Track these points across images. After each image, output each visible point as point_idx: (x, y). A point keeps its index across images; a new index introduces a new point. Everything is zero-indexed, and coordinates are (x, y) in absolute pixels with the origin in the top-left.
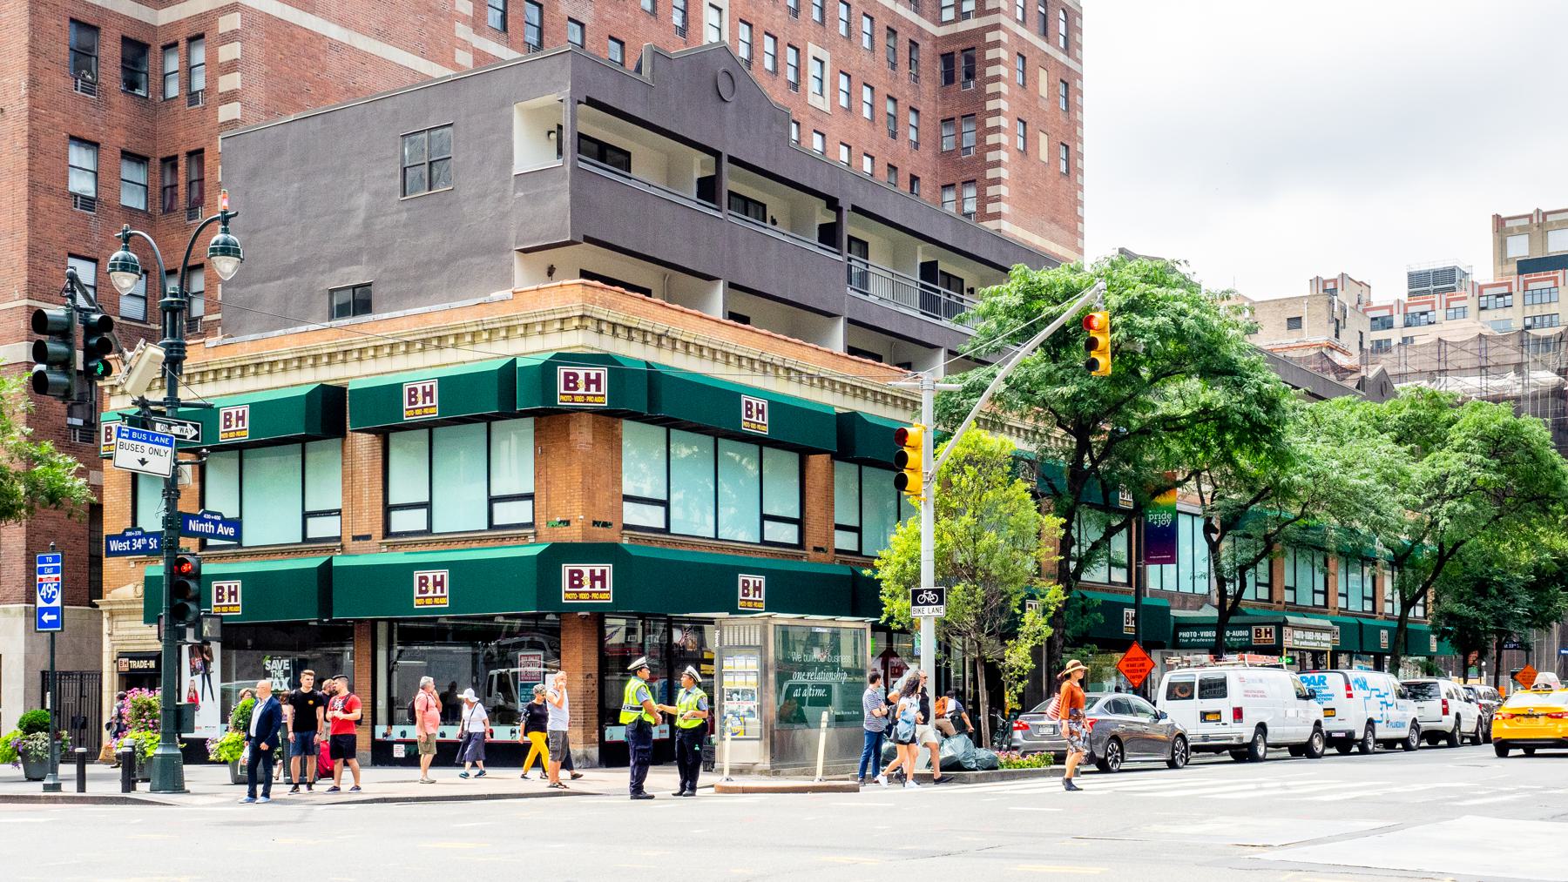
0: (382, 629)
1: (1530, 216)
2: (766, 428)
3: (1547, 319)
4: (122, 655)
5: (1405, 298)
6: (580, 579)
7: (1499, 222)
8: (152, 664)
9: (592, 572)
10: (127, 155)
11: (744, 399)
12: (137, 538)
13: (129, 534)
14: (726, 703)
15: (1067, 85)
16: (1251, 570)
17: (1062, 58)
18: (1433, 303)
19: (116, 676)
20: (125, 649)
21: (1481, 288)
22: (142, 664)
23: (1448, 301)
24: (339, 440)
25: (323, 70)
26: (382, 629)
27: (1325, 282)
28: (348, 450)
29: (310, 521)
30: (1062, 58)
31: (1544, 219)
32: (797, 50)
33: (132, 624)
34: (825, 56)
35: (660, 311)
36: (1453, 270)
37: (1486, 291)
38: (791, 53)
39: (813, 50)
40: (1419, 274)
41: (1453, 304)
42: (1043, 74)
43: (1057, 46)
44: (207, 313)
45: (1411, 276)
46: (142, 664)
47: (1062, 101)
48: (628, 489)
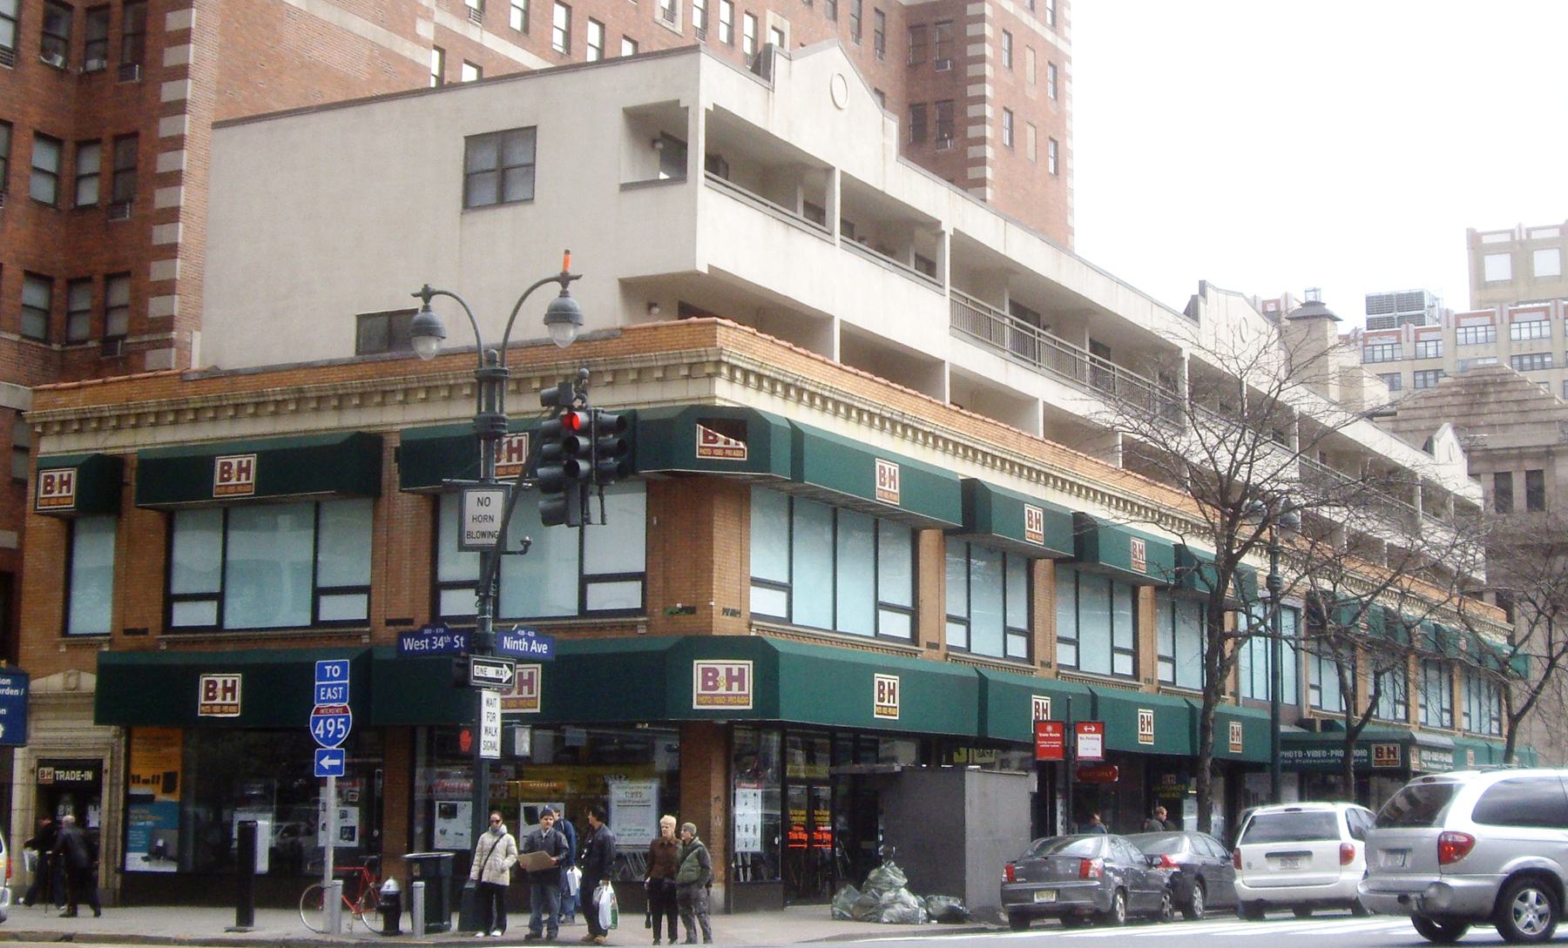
0: (422, 739)
1: (1512, 232)
2: (897, 498)
3: (1526, 361)
4: (43, 763)
5: (1363, 325)
6: (714, 679)
7: (1474, 240)
8: (89, 775)
9: (729, 671)
10: (41, 136)
11: (878, 463)
12: (439, 636)
13: (427, 631)
14: (440, 823)
15: (1055, 68)
16: (1387, 675)
17: (1049, 36)
18: (1398, 334)
19: (33, 792)
20: (48, 755)
21: (1458, 317)
22: (75, 776)
23: (1417, 332)
24: (367, 503)
25: (279, 42)
26: (422, 739)
27: (1265, 304)
28: (384, 513)
29: (217, 589)
30: (1049, 36)
31: (1528, 235)
32: (755, 19)
33: (77, 724)
34: (786, 26)
35: (788, 355)
36: (1420, 295)
37: (1464, 322)
38: (748, 21)
39: (771, 18)
40: (1379, 298)
41: (1423, 336)
42: (1030, 55)
43: (1043, 22)
44: (131, 333)
45: (1369, 299)
46: (75, 776)
47: (1050, 87)
48: (755, 573)
